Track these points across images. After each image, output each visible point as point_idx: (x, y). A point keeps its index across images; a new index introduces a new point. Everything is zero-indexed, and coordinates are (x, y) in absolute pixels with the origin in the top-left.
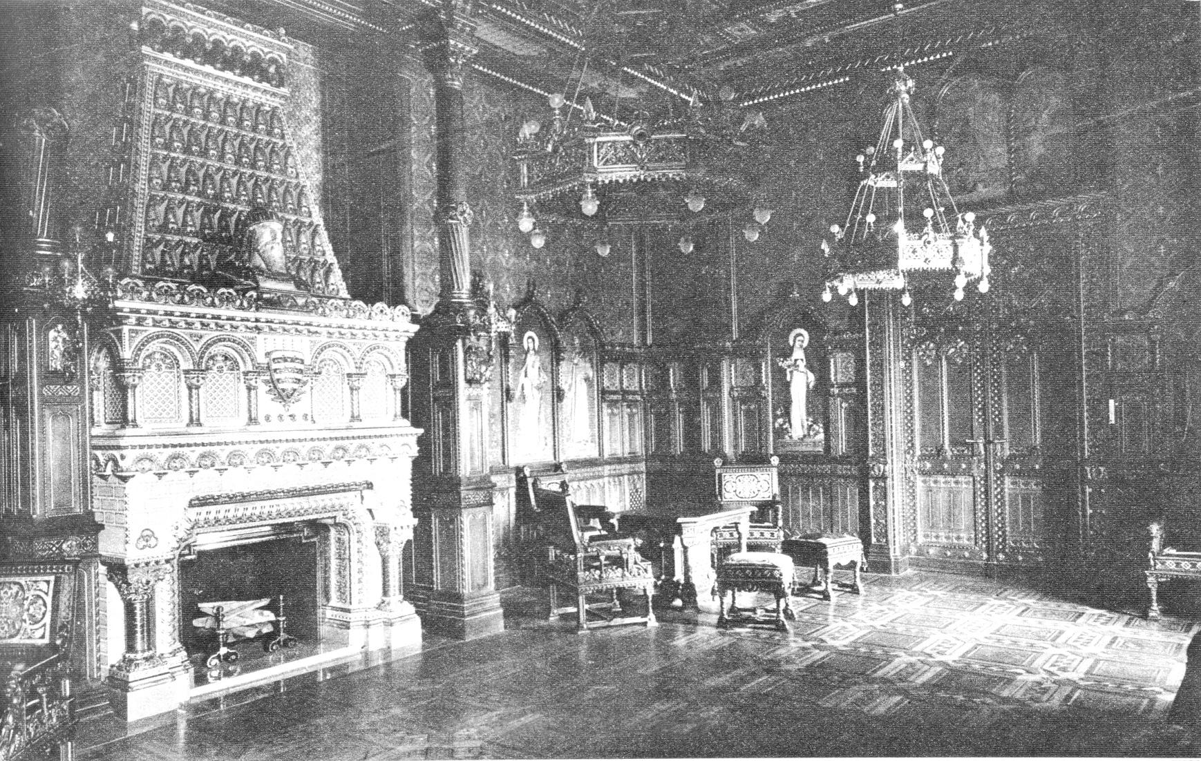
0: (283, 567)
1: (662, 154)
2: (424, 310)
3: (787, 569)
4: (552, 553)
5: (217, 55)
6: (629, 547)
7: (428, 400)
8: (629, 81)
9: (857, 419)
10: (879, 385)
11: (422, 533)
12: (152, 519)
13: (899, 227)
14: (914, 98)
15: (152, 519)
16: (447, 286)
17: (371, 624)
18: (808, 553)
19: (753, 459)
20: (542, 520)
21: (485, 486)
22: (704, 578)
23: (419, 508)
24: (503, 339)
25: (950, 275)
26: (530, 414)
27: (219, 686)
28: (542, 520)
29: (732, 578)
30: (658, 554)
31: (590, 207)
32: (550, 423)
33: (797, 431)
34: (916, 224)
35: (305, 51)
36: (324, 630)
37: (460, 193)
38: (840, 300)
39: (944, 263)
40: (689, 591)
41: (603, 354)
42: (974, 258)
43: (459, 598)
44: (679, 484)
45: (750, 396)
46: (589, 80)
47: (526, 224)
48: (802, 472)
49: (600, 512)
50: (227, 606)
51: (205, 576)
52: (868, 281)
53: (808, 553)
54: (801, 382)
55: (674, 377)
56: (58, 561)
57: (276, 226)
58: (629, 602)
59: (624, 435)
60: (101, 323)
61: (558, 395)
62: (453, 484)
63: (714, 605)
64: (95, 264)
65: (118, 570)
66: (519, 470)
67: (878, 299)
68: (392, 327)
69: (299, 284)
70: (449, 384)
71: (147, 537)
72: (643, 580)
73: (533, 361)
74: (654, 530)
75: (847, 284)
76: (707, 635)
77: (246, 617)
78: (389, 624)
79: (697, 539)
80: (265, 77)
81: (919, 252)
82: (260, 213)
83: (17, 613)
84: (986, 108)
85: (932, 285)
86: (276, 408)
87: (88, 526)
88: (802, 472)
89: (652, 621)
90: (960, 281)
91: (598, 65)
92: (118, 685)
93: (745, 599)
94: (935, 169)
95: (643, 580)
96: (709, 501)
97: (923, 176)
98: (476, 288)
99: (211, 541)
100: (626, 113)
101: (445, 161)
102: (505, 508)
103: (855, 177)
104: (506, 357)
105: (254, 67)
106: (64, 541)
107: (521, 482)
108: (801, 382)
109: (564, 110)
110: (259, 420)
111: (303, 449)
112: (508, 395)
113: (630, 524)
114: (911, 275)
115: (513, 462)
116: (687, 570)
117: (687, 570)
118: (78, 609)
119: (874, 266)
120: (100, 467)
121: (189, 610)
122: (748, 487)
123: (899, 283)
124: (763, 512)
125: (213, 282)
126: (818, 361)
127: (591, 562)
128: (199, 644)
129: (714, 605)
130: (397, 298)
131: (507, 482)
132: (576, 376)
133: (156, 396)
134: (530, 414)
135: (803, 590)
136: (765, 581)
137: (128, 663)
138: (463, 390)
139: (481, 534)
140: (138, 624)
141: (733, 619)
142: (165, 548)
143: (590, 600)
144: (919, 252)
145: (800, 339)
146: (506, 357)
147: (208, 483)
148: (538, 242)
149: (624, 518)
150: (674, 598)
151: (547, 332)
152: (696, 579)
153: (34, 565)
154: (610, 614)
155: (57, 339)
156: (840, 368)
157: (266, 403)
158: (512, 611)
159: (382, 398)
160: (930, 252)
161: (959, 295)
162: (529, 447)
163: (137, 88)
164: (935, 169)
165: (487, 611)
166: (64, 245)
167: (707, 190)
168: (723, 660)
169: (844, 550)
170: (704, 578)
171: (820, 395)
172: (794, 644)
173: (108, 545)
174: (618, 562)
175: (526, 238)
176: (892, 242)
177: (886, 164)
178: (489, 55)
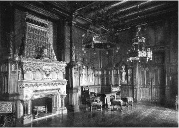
0: (48, 102)
1: (104, 39)
2: (68, 62)
3: (121, 101)
4: (87, 100)
5: (37, 23)
6: (98, 99)
7: (68, 77)
8: (98, 27)
9: (132, 79)
10: (135, 74)
11: (67, 96)
12: (28, 94)
13: (139, 50)
14: (141, 30)
15: (28, 94)
16: (71, 59)
17: (60, 110)
18: (125, 100)
19: (116, 85)
20: (85, 94)
21: (77, 89)
22: (109, 103)
23: (67, 92)
24: (80, 67)
25: (146, 57)
26: (83, 78)
27: (37, 119)
28: (85, 94)
29: (113, 103)
30: (103, 100)
31: (93, 47)
32: (87, 80)
33: (123, 81)
34: (141, 50)
35: (51, 23)
36: (53, 111)
37: (73, 44)
38: (130, 61)
39: (145, 56)
40: (107, 105)
41: (93, 69)
42: (150, 54)
43: (73, 106)
44: (106, 89)
45: (116, 76)
46: (92, 27)
47: (83, 49)
48: (123, 87)
49: (94, 93)
50: (38, 107)
51: (36, 103)
52: (134, 58)
53: (125, 100)
54: (124, 73)
55: (105, 72)
56: (13, 100)
57: (46, 49)
58: (98, 107)
59: (98, 82)
60: (21, 64)
61: (88, 75)
62: (72, 89)
63: (111, 107)
64: (19, 55)
65: (22, 101)
66: (82, 87)
67: (136, 61)
68: (64, 65)
69: (50, 58)
70: (71, 74)
71: (27, 96)
72: (100, 104)
73: (84, 71)
74: (102, 96)
75: (131, 59)
76: (110, 112)
77: (42, 109)
78: (63, 110)
79: (108, 97)
80: (45, 27)
81: (141, 54)
82: (44, 48)
83: (7, 107)
84: (151, 33)
85: (143, 59)
86: (46, 77)
87: (18, 95)
88: (123, 87)
89: (101, 110)
90: (148, 58)
91: (94, 25)
92: (22, 119)
93: (115, 107)
94: (144, 41)
95: (100, 104)
96: (110, 91)
97: (142, 42)
98: (76, 59)
99: (36, 97)
100: (98, 33)
101: (71, 39)
102: (80, 93)
103: (132, 43)
104: (80, 70)
105: (43, 25)
106: (15, 97)
107: (82, 89)
108: (124, 73)
109: (89, 32)
110: (42, 80)
111: (46, 83)
112: (80, 75)
113: (98, 95)
114: (141, 57)
115: (81, 85)
116: (107, 102)
117: (107, 102)
118: (16, 107)
119: (134, 56)
120: (20, 85)
121: (33, 108)
122: (115, 89)
123: (139, 59)
124: (118, 93)
125: (37, 58)
126: (126, 70)
127: (93, 101)
128: (34, 113)
129: (111, 107)
130: (64, 61)
131: (80, 88)
132: (90, 72)
133: (29, 76)
134: (83, 78)
135: (124, 105)
136: (119, 103)
137: (24, 115)
138: (73, 75)
139: (76, 97)
140: (25, 110)
141: (113, 110)
142: (29, 98)
143: (93, 106)
144: (141, 54)
145: (124, 67)
146: (80, 70)
147: (36, 88)
148: (85, 52)
149: (97, 94)
150: (105, 106)
151: (86, 66)
152: (108, 104)
153: (9, 101)
154: (95, 109)
155: (13, 66)
156: (129, 72)
157: (45, 76)
158: (81, 108)
159: (61, 76)
160: (143, 54)
161: (147, 61)
162: (84, 83)
163: (26, 28)
164: (144, 41)
165: (77, 109)
166: (15, 53)
167: (110, 44)
168: (112, 116)
169: (130, 99)
170: (109, 103)
171: (127, 75)
172: (123, 113)
173: (20, 98)
174: (97, 101)
175: (83, 51)
176: (137, 53)
177: (137, 41)
178: (78, 24)
